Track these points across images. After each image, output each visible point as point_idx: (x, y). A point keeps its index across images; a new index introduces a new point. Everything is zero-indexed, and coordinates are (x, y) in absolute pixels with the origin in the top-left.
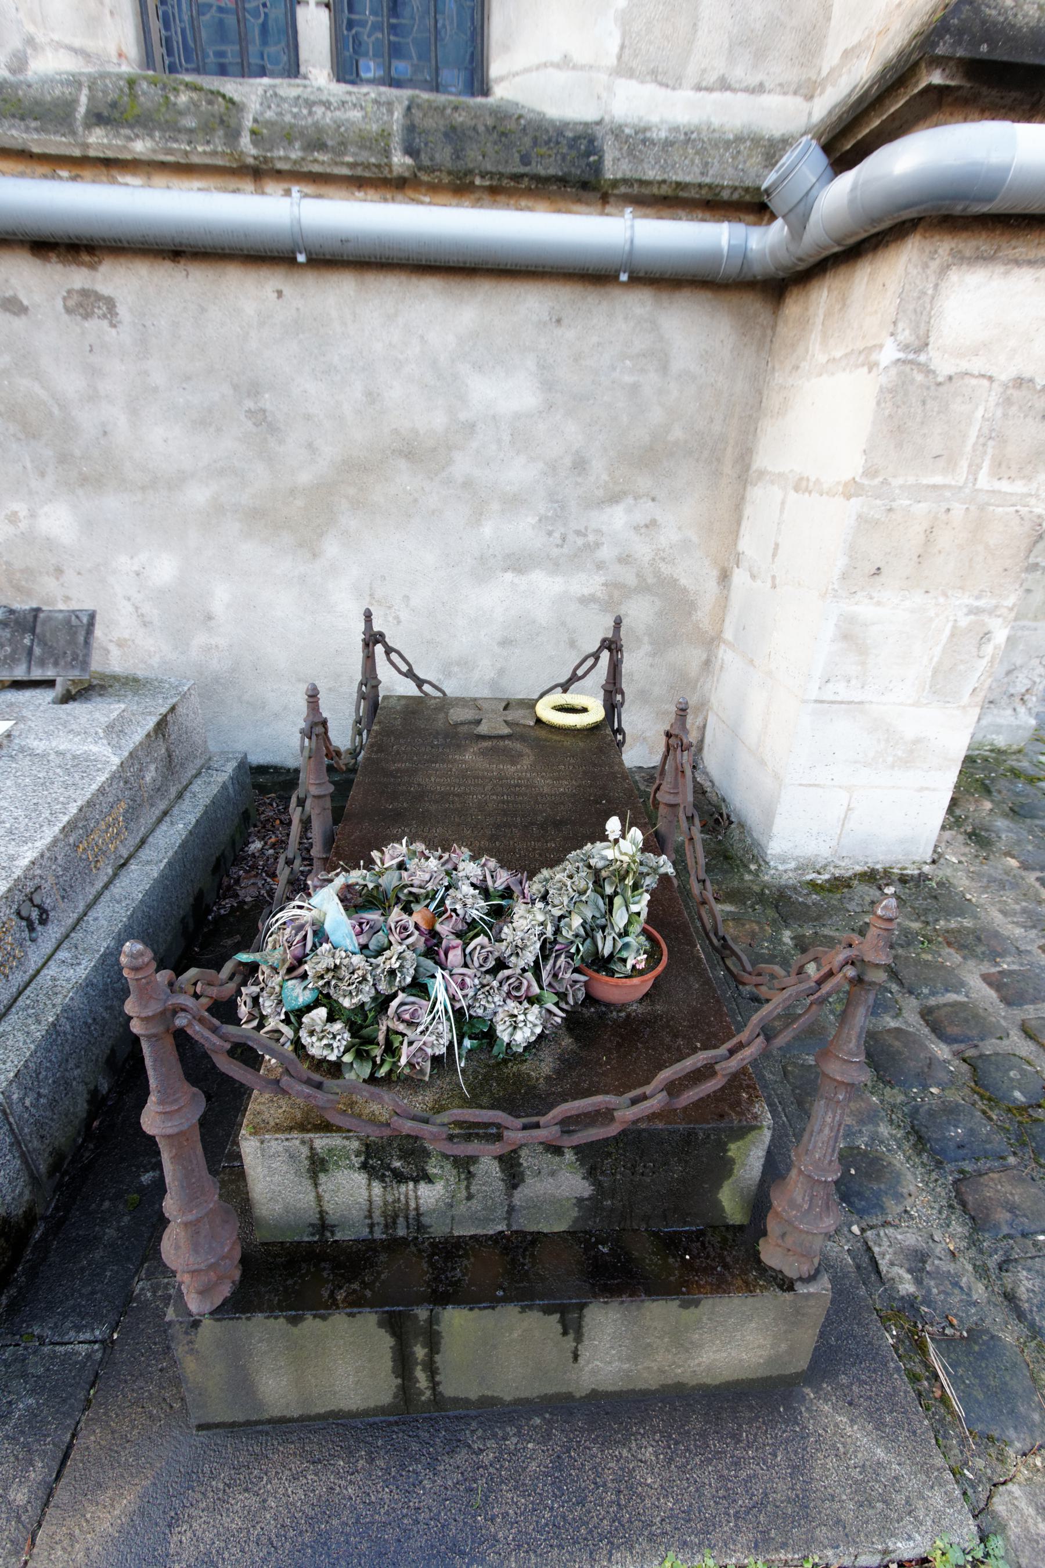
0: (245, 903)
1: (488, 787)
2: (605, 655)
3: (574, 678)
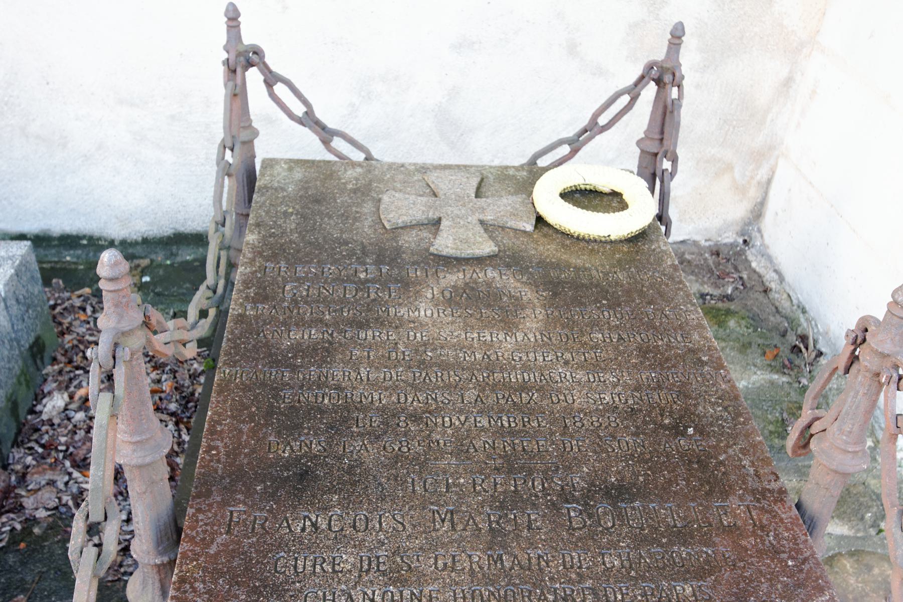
0: (34, 521)
1: (471, 395)
2: (650, 91)
3: (592, 129)
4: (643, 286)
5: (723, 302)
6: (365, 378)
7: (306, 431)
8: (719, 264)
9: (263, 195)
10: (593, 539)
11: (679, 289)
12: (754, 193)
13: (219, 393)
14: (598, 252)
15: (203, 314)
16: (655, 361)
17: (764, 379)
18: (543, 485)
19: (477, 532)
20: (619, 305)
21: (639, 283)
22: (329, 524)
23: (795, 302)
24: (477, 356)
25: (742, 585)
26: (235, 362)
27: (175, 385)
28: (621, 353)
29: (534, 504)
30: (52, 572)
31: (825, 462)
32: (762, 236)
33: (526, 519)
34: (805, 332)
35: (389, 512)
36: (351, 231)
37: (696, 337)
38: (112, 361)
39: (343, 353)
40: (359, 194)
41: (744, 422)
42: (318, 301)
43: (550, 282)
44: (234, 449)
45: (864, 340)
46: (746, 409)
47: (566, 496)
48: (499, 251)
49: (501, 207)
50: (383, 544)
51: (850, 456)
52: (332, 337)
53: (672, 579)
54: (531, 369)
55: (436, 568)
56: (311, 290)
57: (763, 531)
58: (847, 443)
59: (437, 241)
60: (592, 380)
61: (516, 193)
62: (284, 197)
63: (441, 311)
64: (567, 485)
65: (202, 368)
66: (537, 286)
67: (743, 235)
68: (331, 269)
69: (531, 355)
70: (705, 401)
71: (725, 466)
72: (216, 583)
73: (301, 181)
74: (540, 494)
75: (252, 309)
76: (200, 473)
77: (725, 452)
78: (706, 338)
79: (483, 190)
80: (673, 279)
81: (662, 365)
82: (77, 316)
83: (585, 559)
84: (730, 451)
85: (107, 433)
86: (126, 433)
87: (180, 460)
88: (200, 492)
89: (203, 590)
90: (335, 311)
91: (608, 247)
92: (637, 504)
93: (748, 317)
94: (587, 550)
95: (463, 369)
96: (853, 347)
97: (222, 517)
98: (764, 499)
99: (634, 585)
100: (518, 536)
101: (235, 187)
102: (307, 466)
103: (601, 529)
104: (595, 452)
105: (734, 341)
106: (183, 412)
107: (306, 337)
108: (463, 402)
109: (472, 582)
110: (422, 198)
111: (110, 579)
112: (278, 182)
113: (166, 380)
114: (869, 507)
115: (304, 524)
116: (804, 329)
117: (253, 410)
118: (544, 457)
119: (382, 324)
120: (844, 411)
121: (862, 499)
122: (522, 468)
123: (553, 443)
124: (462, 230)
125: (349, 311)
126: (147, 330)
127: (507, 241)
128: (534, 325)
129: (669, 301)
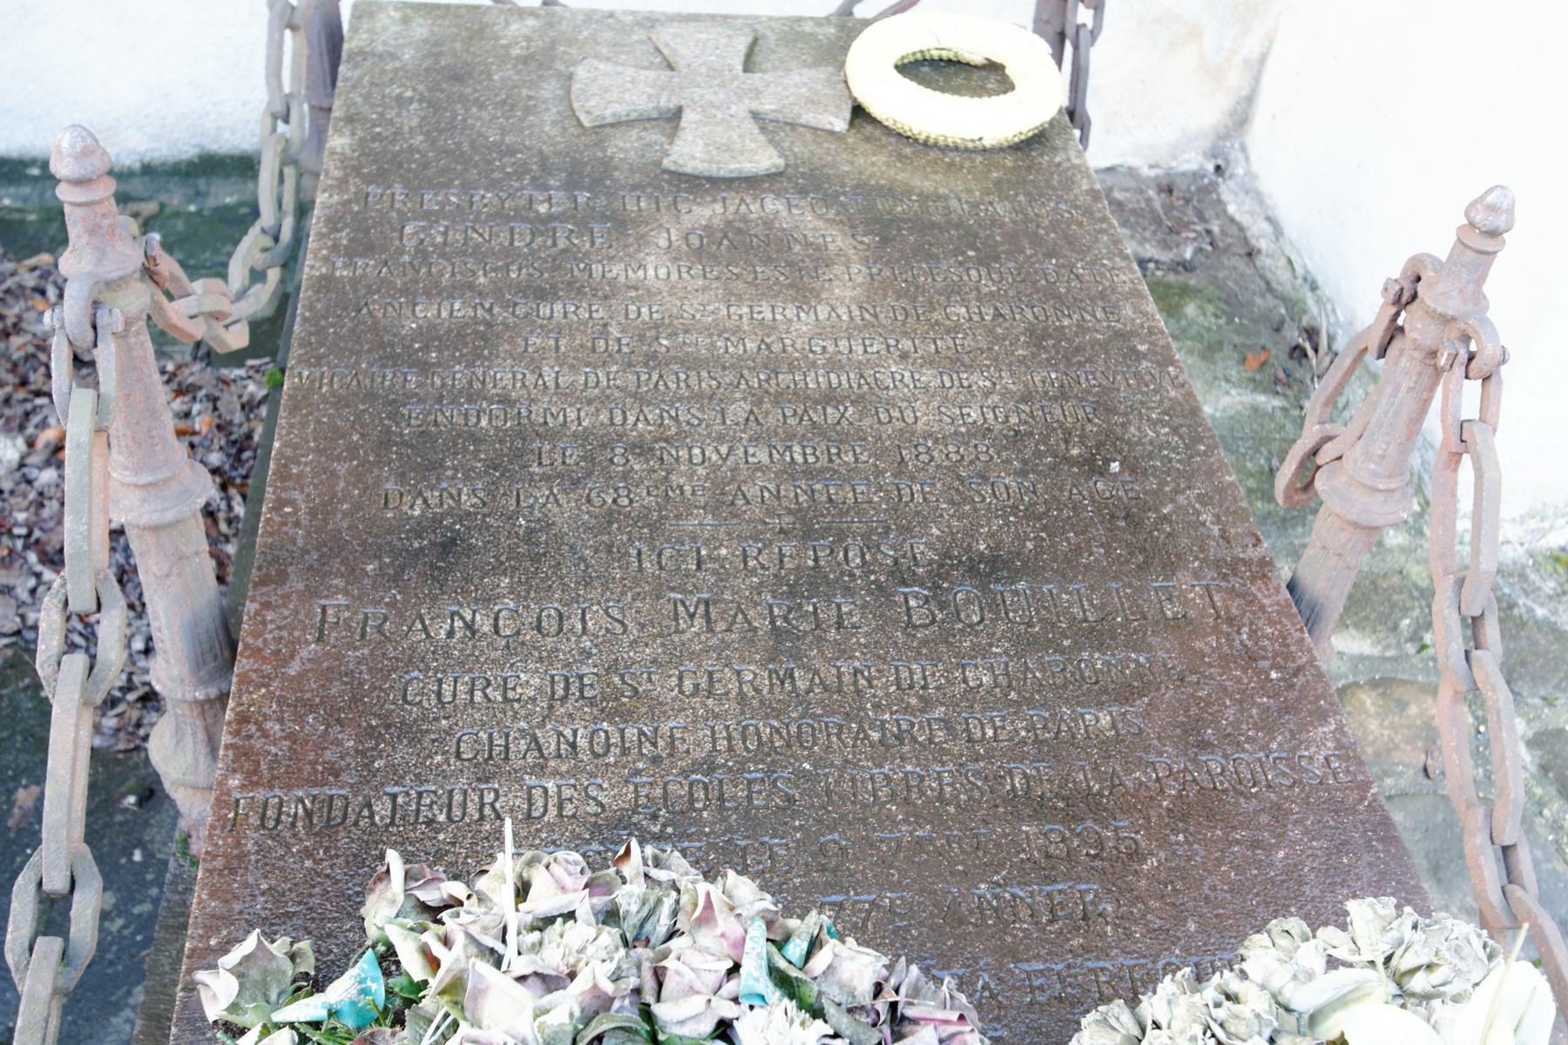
1: (738, 410)
4: (1038, 226)
5: (1176, 272)
6: (551, 384)
7: (449, 473)
8: (1172, 207)
9: (356, 66)
10: (946, 641)
11: (1101, 231)
12: (1236, 81)
13: (294, 409)
14: (962, 167)
15: (257, 276)
16: (1058, 352)
17: (1241, 403)
18: (863, 556)
19: (750, 634)
20: (997, 259)
21: (1031, 221)
22: (496, 626)
23: (1300, 271)
24: (749, 345)
25: (1193, 711)
26: (319, 359)
27: (217, 421)
28: (999, 340)
29: (848, 588)
30: (19, 738)
31: (1338, 509)
32: (1247, 158)
33: (834, 612)
34: (1313, 323)
35: (599, 603)
36: (521, 130)
37: (1128, 311)
38: (91, 332)
39: (511, 341)
40: (533, 66)
41: (1205, 453)
42: (464, 253)
43: (877, 220)
44: (324, 504)
45: (1414, 297)
46: (1210, 430)
47: (901, 575)
48: (787, 166)
49: (789, 87)
50: (590, 655)
51: (1380, 497)
52: (492, 316)
53: (1078, 704)
54: (842, 367)
55: (681, 692)
56: (451, 233)
57: (1231, 625)
58: (1376, 475)
59: (676, 148)
60: (948, 384)
61: (816, 64)
62: (396, 70)
63: (684, 270)
64: (904, 556)
65: (263, 392)
66: (852, 227)
67: (1215, 157)
68: (485, 197)
69: (843, 344)
70: (1141, 418)
71: (1170, 522)
72: (300, 719)
73: (426, 41)
74: (858, 572)
75: (345, 266)
76: (265, 545)
77: (1172, 501)
78: (1145, 314)
79: (757, 58)
80: (1091, 214)
81: (1068, 359)
82: (30, 303)
83: (933, 675)
84: (1181, 499)
85: (90, 460)
86: (126, 468)
87: (231, 549)
88: (267, 575)
89: (280, 734)
90: (495, 270)
91: (979, 159)
92: (1022, 585)
93: (1219, 299)
94: (935, 659)
95: (724, 368)
96: (1394, 310)
97: (307, 615)
98: (1235, 575)
99: (1015, 713)
100: (820, 639)
101: (305, 52)
102: (453, 531)
103: (960, 626)
104: (952, 502)
105: (1193, 339)
106: (233, 468)
107: (444, 314)
108: (724, 423)
109: (743, 713)
110: (647, 73)
111: (121, 746)
112: (385, 43)
113: (199, 413)
114: (1408, 610)
115: (452, 626)
116: (1313, 318)
117: (355, 438)
118: (866, 512)
119: (580, 291)
120: (1374, 420)
121: (1395, 597)
122: (827, 530)
123: (880, 489)
124: (720, 129)
125: (520, 269)
126: (153, 285)
127: (801, 148)
128: (849, 293)
129: (1083, 252)
